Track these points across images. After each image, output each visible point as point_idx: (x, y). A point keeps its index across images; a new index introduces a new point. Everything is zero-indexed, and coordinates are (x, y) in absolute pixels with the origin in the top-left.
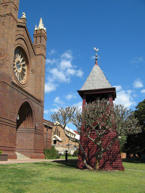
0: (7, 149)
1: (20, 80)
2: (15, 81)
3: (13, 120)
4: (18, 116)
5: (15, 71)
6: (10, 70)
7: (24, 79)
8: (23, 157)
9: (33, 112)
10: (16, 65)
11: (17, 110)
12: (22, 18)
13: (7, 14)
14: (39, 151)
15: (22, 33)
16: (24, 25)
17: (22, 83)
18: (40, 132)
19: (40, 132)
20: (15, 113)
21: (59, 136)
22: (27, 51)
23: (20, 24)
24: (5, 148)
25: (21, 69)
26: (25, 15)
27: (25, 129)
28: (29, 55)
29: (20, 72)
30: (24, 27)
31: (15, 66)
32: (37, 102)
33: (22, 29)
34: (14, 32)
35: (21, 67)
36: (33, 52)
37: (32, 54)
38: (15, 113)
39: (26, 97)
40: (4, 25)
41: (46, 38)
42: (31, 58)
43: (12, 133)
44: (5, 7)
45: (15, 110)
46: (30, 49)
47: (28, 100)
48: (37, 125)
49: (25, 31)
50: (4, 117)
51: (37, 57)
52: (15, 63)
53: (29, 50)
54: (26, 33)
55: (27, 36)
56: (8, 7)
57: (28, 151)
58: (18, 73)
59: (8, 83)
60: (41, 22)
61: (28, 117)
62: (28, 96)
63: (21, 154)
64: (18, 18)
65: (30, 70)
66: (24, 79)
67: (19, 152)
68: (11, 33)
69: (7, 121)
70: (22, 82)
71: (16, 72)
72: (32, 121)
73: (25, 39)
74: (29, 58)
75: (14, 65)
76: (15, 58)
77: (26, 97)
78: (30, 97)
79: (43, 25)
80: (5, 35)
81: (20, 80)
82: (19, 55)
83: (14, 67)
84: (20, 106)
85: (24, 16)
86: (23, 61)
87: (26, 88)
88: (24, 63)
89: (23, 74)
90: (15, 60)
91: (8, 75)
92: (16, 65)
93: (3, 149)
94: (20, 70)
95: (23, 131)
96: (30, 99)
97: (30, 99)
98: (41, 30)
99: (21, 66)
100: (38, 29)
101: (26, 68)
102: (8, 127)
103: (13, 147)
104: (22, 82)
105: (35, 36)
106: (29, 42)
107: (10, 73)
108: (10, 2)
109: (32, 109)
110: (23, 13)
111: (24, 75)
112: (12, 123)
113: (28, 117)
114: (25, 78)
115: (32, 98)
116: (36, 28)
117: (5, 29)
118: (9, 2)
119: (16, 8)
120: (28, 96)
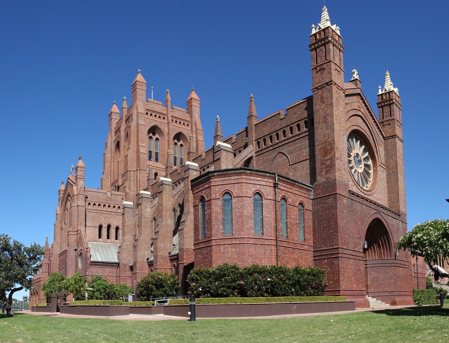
0: (354, 293)
1: (363, 185)
2: (354, 189)
3: (358, 250)
4: (366, 242)
5: (353, 171)
6: (344, 173)
7: (370, 181)
8: (379, 303)
9: (390, 234)
10: (353, 162)
11: (363, 235)
12: (353, 79)
13: (325, 84)
14: (404, 293)
15: (355, 106)
16: (358, 91)
17: (367, 189)
18: (405, 263)
19: (405, 263)
20: (359, 238)
21: (443, 267)
22: (369, 134)
23: (351, 92)
24: (351, 293)
25: (362, 166)
26: (356, 73)
27: (380, 262)
28: (372, 141)
29: (361, 170)
30: (359, 94)
31: (353, 164)
32: (394, 216)
33: (355, 98)
34: (342, 109)
35: (363, 162)
36: (379, 133)
37: (378, 138)
38: (359, 238)
39: (374, 211)
40: (323, 102)
41: (400, 105)
42: (376, 144)
43: (359, 270)
44: (320, 72)
45: (360, 234)
46: (373, 128)
47: (379, 216)
48: (397, 253)
49: (361, 101)
50: (345, 247)
51: (387, 141)
52: (352, 158)
53: (372, 132)
54: (363, 105)
55: (365, 108)
56: (326, 72)
57: (387, 294)
58: (358, 173)
59: (344, 194)
60: (388, 77)
61: (369, 253)
62: (378, 208)
63: (377, 300)
64: (345, 81)
65: (378, 165)
66: (370, 181)
67: (373, 297)
68: (337, 113)
69: (349, 251)
70: (367, 187)
71: (355, 172)
72: (389, 247)
73: (362, 115)
74: (373, 145)
75: (350, 162)
76: (350, 149)
77: (374, 211)
78: (382, 210)
79: (392, 83)
80: (328, 119)
81: (363, 185)
82: (357, 141)
83: (351, 165)
84: (367, 226)
85: (356, 76)
86: (365, 151)
87: (375, 195)
88: (367, 154)
89: (367, 174)
90: (351, 154)
91: (342, 182)
92: (353, 162)
93: (347, 294)
94: (361, 170)
95: (377, 265)
96: (382, 214)
97: (382, 214)
98: (389, 93)
99: (362, 160)
100: (383, 92)
101: (370, 162)
102: (352, 261)
103: (362, 290)
104: (367, 187)
105: (380, 105)
106: (371, 118)
107: (344, 177)
108: (327, 63)
109: (387, 228)
110: (353, 71)
111: (368, 174)
112: (358, 254)
113: (369, 253)
114: (371, 179)
115: (385, 211)
116: (380, 90)
117: (326, 109)
118: (326, 63)
119: (339, 69)
120: (378, 209)
